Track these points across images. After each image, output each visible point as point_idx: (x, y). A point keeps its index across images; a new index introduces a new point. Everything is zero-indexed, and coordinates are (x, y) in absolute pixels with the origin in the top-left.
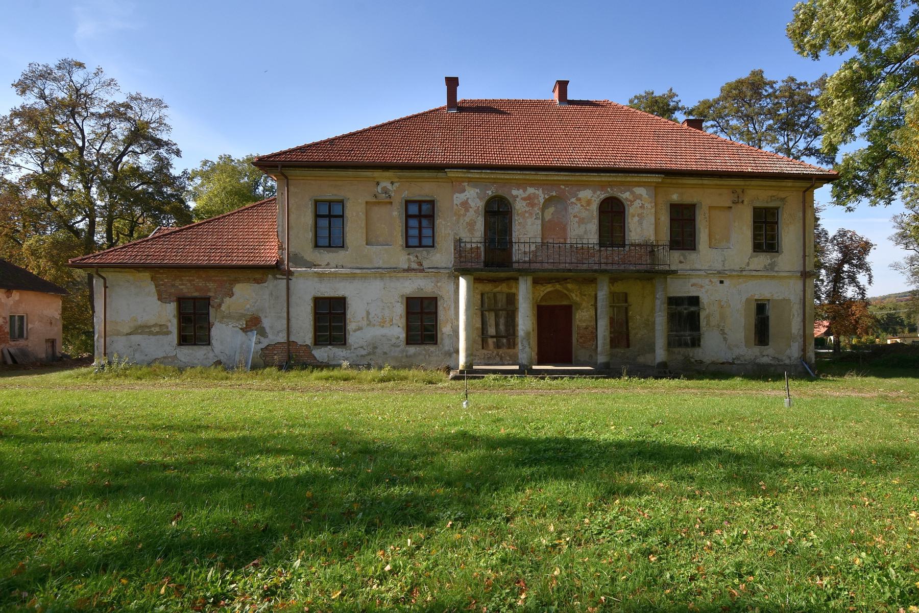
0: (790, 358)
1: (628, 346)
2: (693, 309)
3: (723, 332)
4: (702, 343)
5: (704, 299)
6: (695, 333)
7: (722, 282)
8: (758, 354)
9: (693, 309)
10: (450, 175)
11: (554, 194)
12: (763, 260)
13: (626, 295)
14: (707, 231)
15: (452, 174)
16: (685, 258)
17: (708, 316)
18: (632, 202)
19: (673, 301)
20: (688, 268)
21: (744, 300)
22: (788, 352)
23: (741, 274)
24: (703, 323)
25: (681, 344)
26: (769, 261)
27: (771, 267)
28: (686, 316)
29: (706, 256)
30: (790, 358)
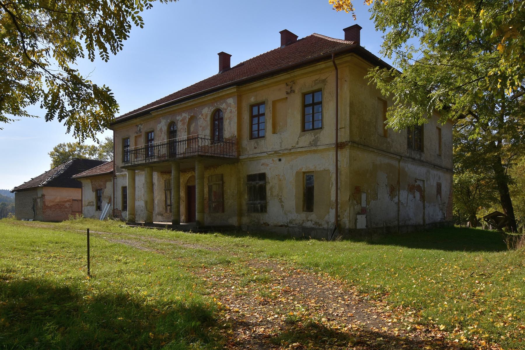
0: (328, 223)
1: (223, 211)
2: (261, 183)
3: (281, 201)
4: (268, 209)
5: (269, 176)
6: (262, 202)
7: (280, 160)
8: (305, 219)
9: (261, 183)
10: (153, 114)
11: (192, 114)
12: (308, 137)
13: (222, 175)
14: (271, 121)
15: (154, 114)
16: (258, 145)
17: (271, 188)
18: (226, 109)
19: (251, 178)
20: (259, 151)
21: (295, 172)
22: (327, 217)
23: (291, 152)
24: (268, 194)
25: (256, 210)
26: (313, 138)
27: (314, 143)
28: (257, 187)
29: (272, 141)
30: (328, 223)
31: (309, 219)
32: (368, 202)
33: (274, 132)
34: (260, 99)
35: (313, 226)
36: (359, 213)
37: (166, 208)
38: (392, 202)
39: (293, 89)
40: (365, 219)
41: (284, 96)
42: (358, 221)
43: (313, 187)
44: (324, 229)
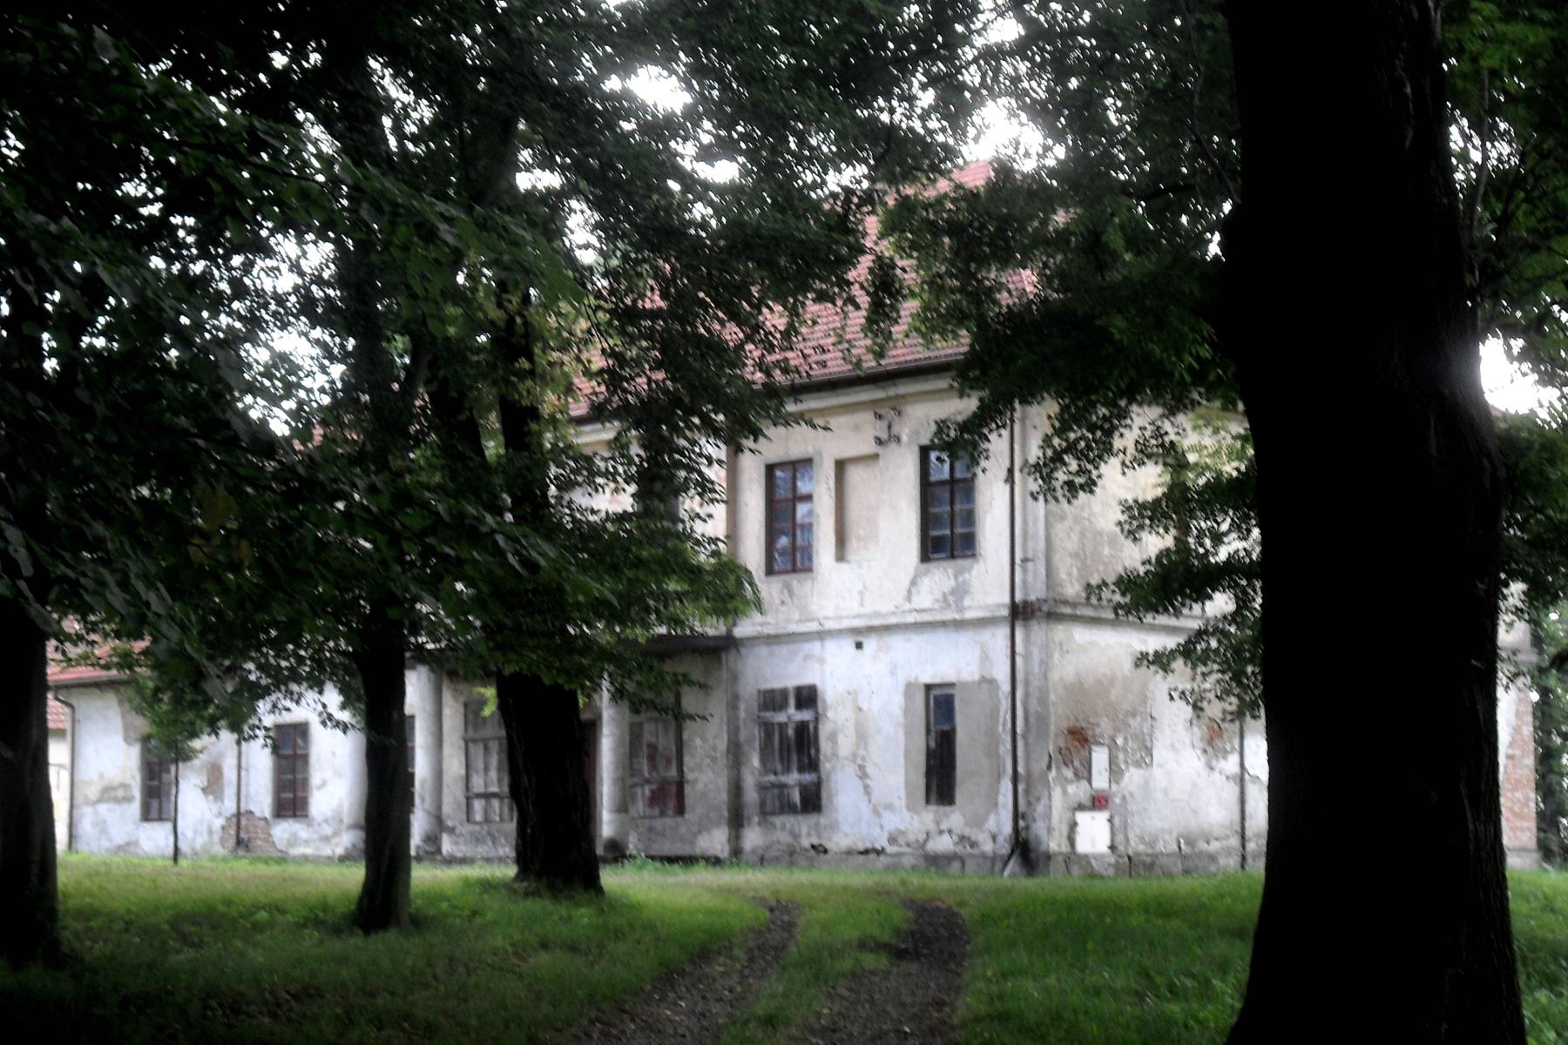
1: (681, 810)
2: (806, 715)
3: (863, 775)
6: (808, 777)
7: (859, 646)
8: (932, 827)
9: (806, 715)
12: (941, 577)
17: (833, 737)
21: (902, 683)
30: (994, 838)
31: (944, 826)
32: (1115, 772)
33: (841, 556)
34: (796, 451)
35: (959, 849)
36: (1081, 807)
37: (469, 807)
38: (1216, 775)
39: (895, 430)
40: (1107, 826)
41: (869, 447)
42: (1079, 829)
43: (953, 730)
44: (984, 856)
